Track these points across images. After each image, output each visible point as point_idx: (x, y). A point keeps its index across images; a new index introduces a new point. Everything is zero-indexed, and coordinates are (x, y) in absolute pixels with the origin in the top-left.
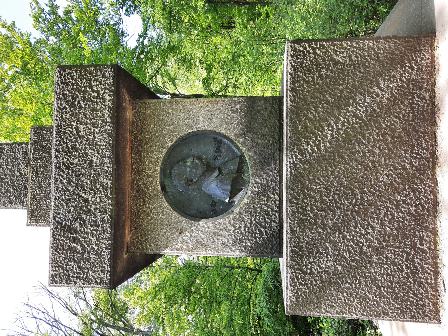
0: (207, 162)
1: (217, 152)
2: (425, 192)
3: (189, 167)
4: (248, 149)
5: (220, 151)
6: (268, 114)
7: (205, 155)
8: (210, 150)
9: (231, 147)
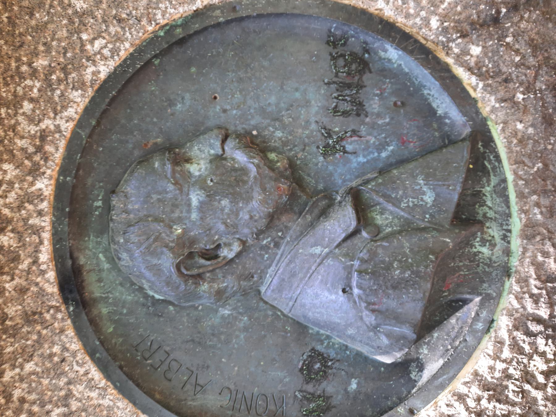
0: (292, 165)
1: (345, 114)
3: (196, 195)
4: (510, 100)
5: (359, 109)
7: (284, 127)
8: (307, 104)
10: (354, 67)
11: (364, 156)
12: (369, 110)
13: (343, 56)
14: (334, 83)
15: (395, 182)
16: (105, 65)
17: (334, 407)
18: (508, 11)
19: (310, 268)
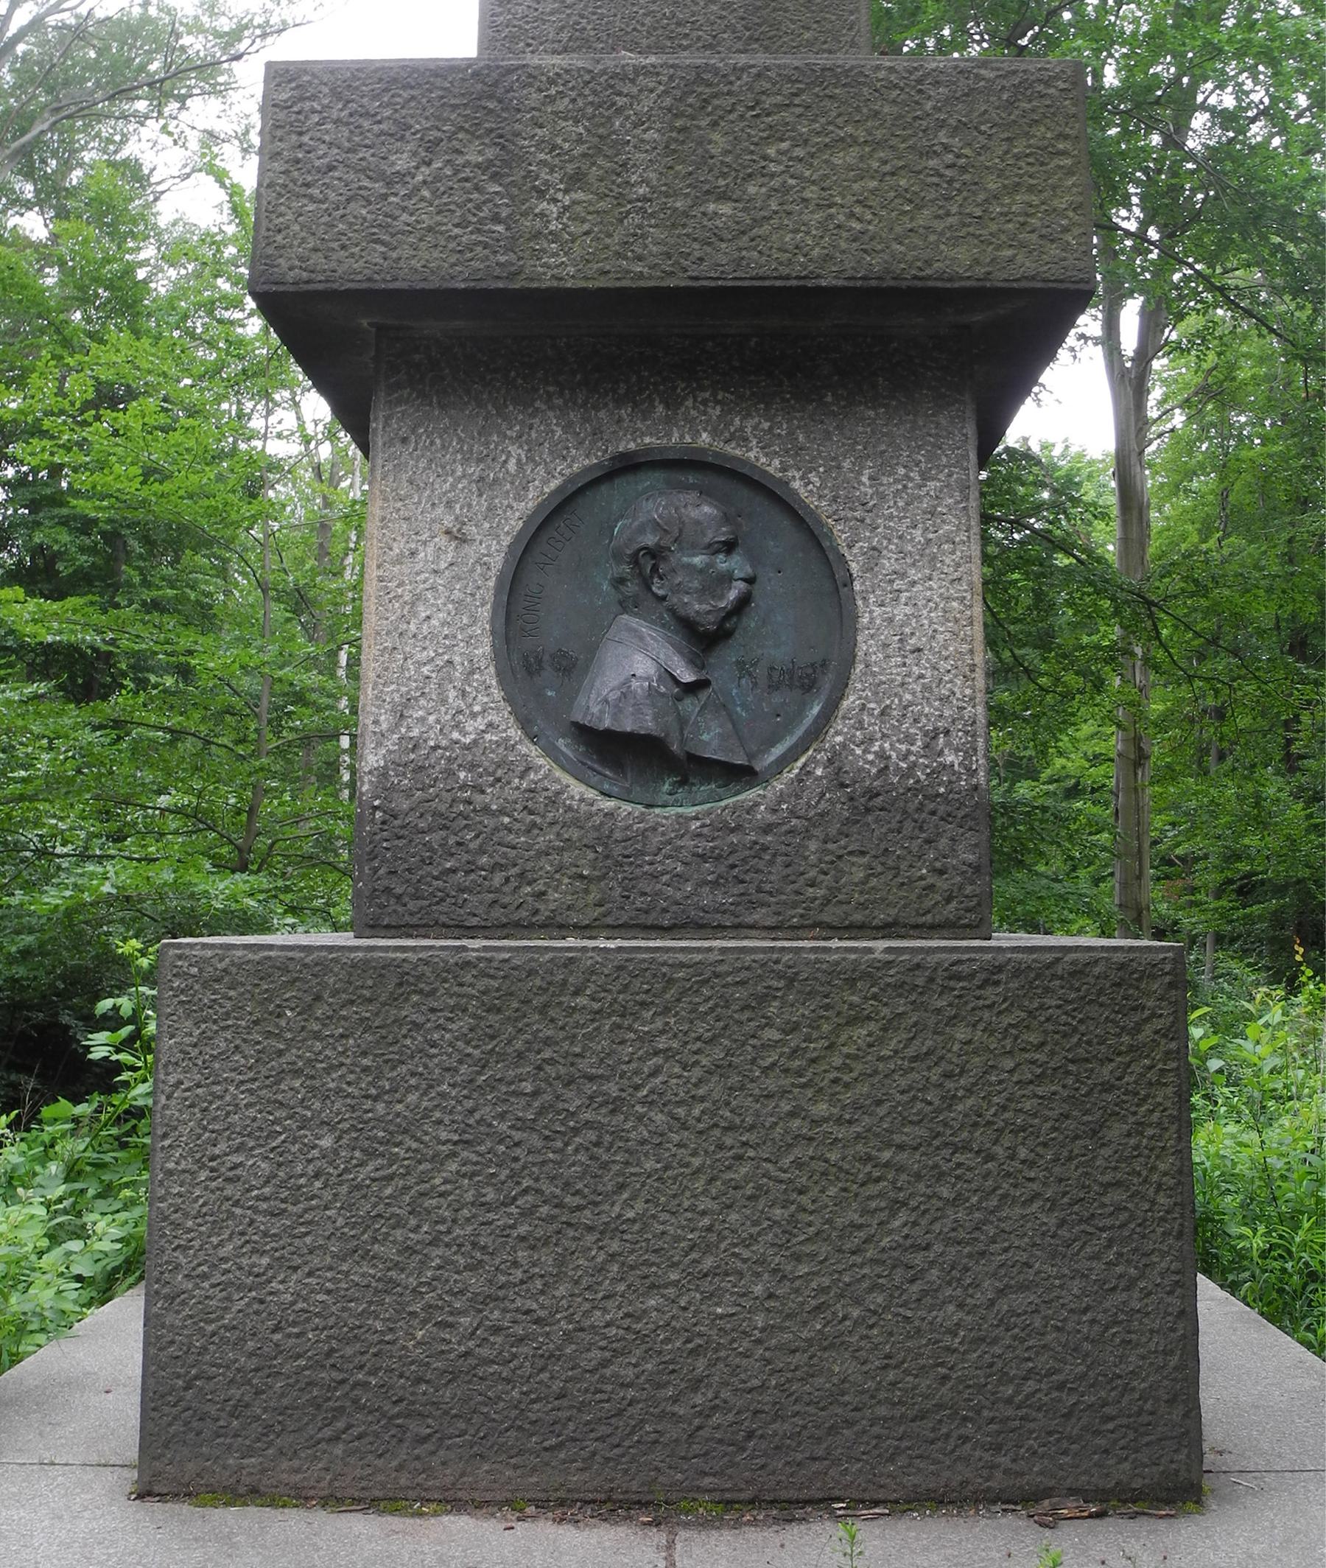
1: (770, 676)
2: (608, 1460)
4: (781, 798)
5: (774, 687)
6: (922, 878)
9: (791, 733)
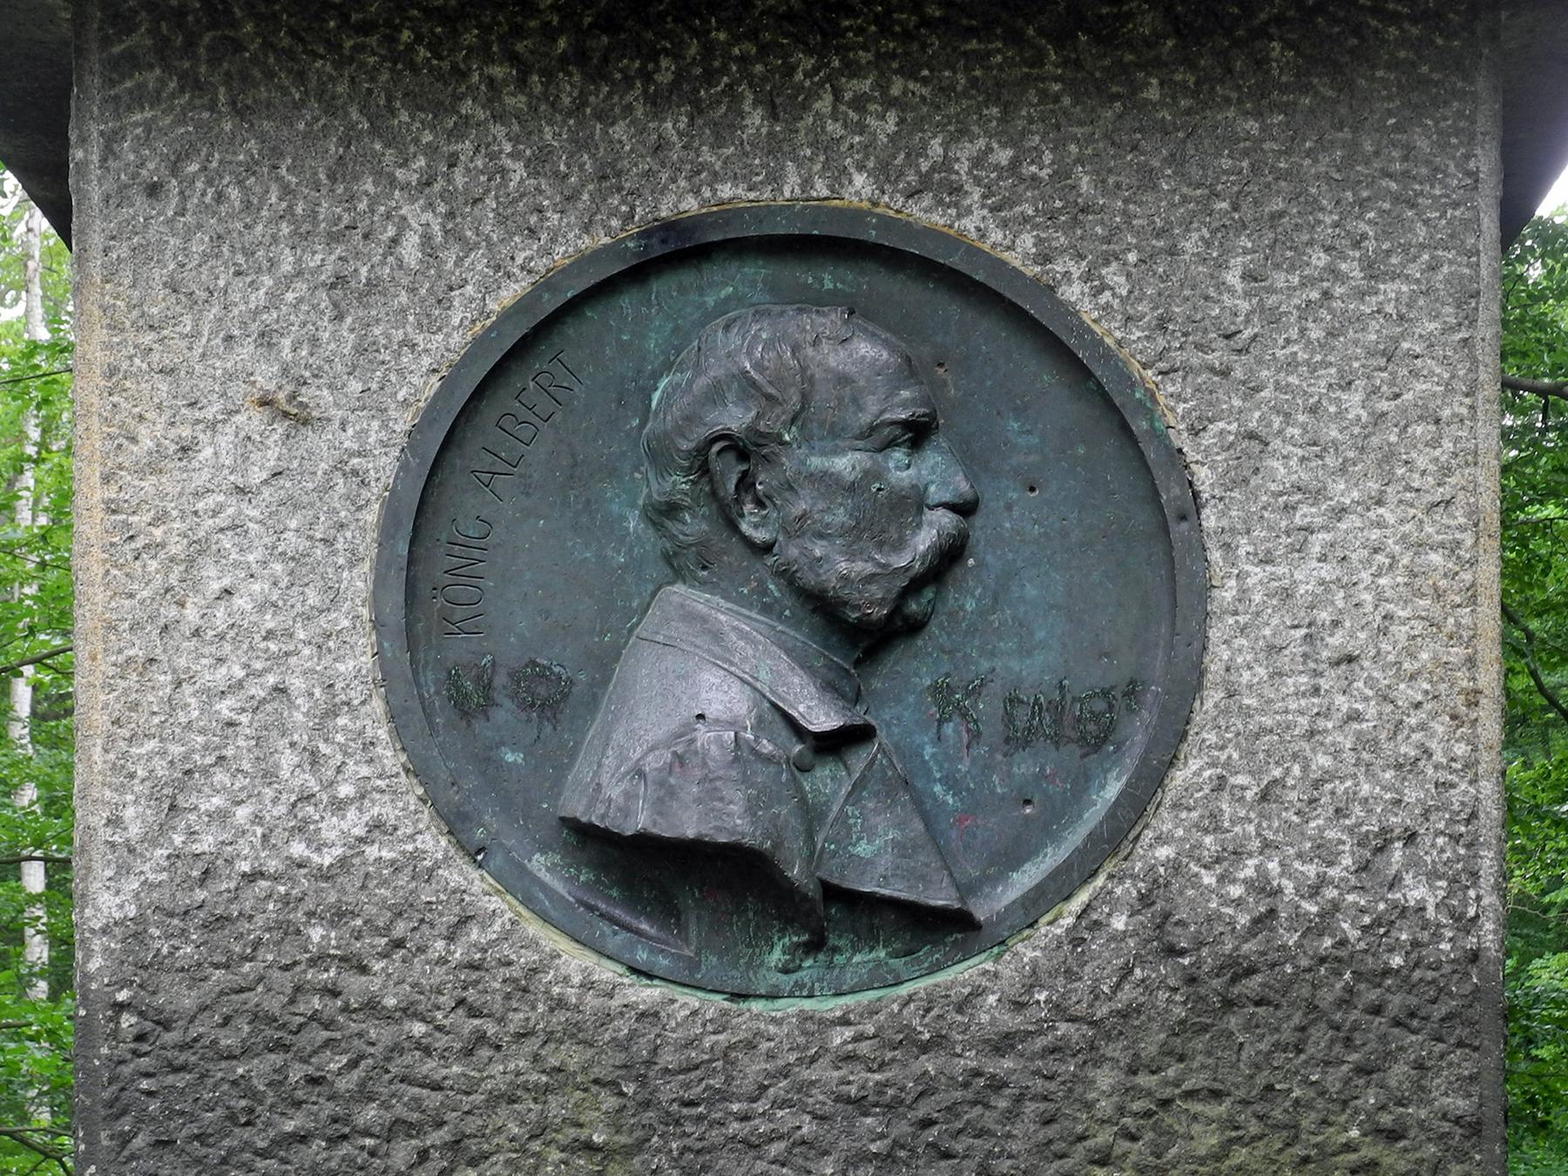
1: (1009, 719)
5: (1017, 740)
7: (982, 613)
8: (1025, 652)
10: (1091, 727)
11: (933, 755)
12: (1017, 757)
13: (1111, 707)
14: (1063, 697)
15: (887, 796)
16: (1083, 293)
17: (469, 724)
18: (1184, 967)
19: (732, 664)
